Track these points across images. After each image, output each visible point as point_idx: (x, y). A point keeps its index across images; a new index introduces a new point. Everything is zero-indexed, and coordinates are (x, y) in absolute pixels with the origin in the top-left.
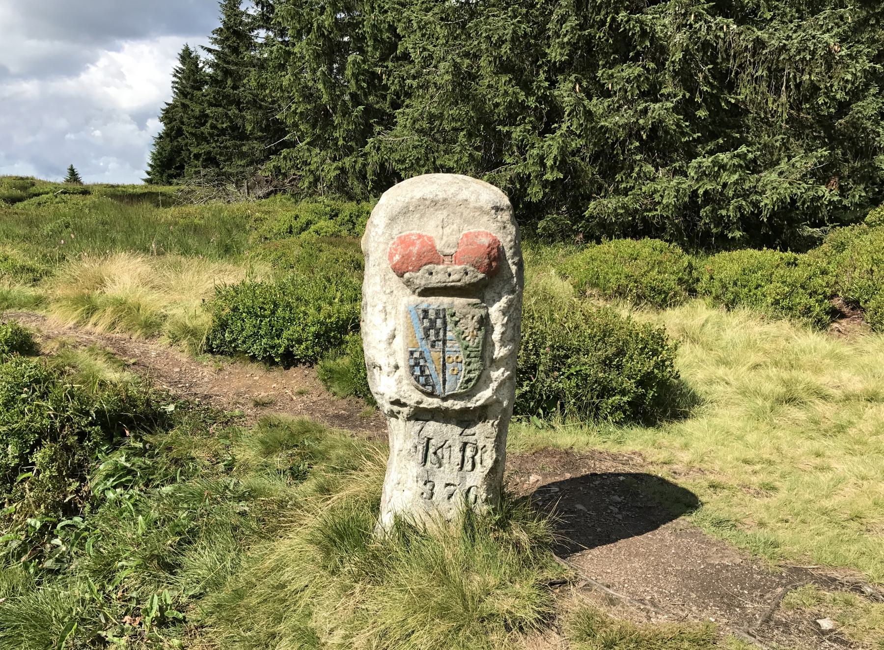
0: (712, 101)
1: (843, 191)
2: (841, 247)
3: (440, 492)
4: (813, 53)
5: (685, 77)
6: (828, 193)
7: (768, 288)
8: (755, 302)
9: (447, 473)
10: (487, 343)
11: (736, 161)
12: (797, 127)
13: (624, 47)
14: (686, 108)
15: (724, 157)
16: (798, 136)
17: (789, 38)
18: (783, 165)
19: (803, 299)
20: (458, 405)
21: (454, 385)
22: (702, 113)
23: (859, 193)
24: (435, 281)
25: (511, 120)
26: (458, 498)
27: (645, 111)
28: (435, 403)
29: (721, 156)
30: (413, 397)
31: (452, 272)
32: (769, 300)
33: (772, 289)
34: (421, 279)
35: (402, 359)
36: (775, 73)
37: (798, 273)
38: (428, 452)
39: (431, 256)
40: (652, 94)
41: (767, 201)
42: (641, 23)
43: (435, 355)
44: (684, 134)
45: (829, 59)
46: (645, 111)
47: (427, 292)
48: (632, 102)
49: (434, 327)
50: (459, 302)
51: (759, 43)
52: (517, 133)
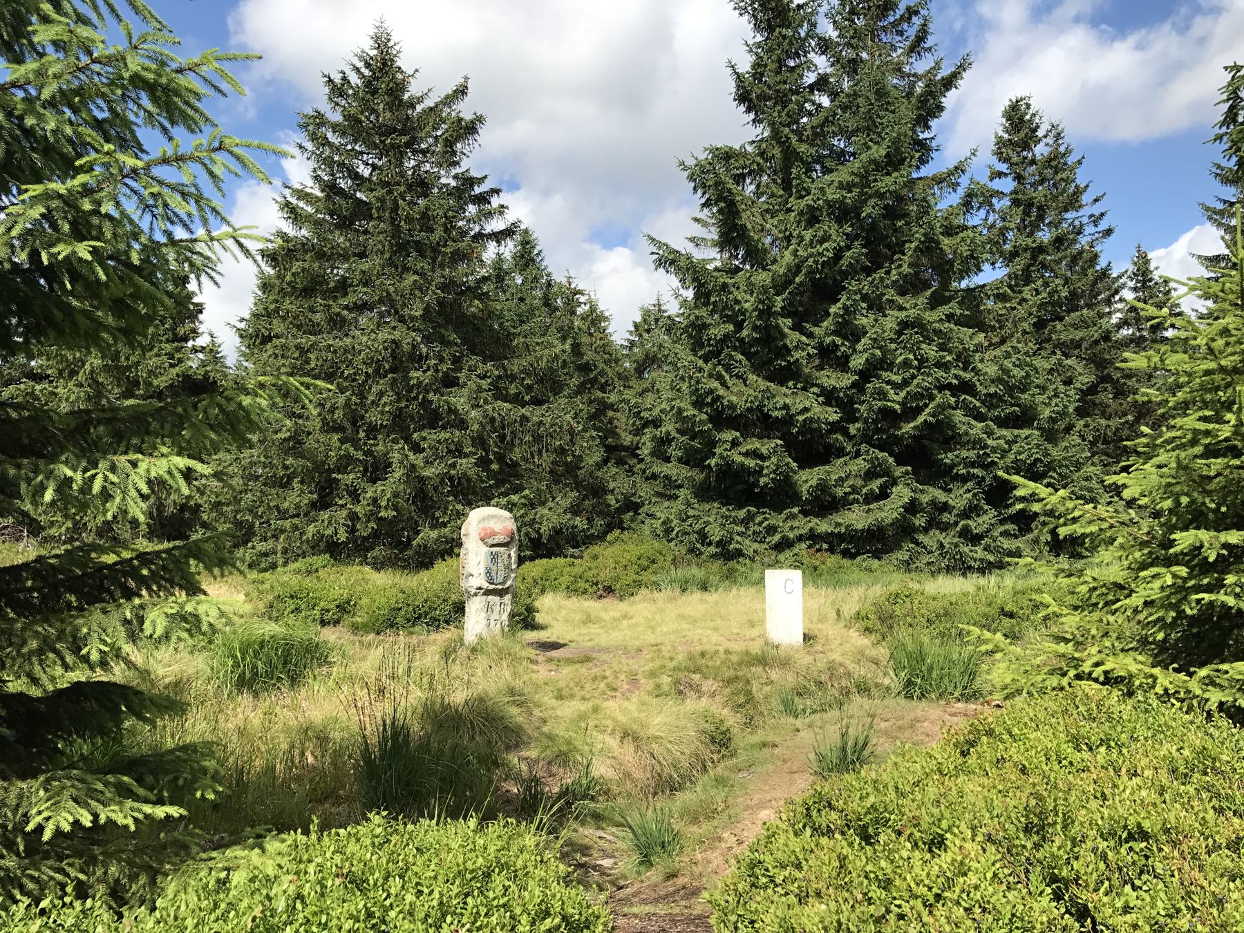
0: (501, 458)
1: (590, 520)
2: (595, 557)
3: (492, 623)
4: (561, 427)
5: (479, 441)
6: (580, 522)
7: (561, 579)
8: (555, 589)
9: (495, 616)
10: (510, 563)
11: (523, 501)
12: (556, 477)
13: (433, 419)
14: (483, 463)
15: (515, 498)
16: (557, 482)
17: (543, 415)
18: (550, 504)
19: (582, 584)
20: (500, 587)
21: (500, 579)
22: (495, 467)
23: (600, 522)
24: (495, 542)
25: (342, 469)
26: (498, 626)
27: (454, 465)
28: (492, 587)
29: (513, 497)
30: (486, 585)
31: (500, 539)
32: (564, 587)
33: (565, 580)
34: (491, 541)
35: (483, 571)
36: (537, 438)
37: (577, 570)
38: (489, 608)
39: (493, 534)
40: (459, 452)
41: (545, 528)
42: (448, 403)
43: (494, 568)
44: (482, 481)
45: (571, 432)
46: (454, 465)
47: (493, 546)
48: (443, 457)
49: (494, 558)
50: (502, 549)
51: (524, 418)
52: (348, 479)
